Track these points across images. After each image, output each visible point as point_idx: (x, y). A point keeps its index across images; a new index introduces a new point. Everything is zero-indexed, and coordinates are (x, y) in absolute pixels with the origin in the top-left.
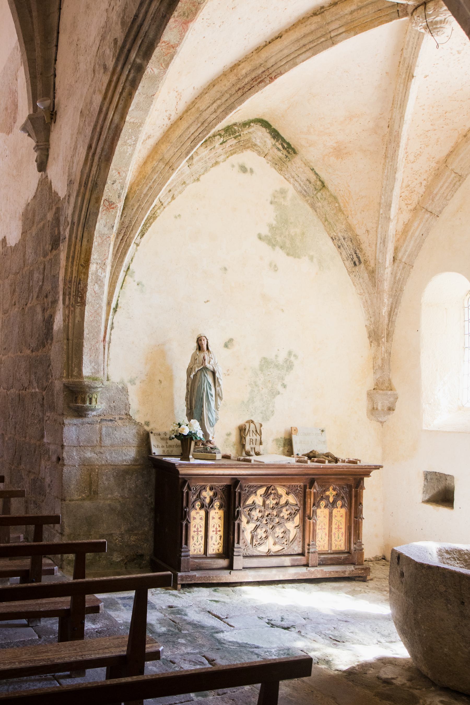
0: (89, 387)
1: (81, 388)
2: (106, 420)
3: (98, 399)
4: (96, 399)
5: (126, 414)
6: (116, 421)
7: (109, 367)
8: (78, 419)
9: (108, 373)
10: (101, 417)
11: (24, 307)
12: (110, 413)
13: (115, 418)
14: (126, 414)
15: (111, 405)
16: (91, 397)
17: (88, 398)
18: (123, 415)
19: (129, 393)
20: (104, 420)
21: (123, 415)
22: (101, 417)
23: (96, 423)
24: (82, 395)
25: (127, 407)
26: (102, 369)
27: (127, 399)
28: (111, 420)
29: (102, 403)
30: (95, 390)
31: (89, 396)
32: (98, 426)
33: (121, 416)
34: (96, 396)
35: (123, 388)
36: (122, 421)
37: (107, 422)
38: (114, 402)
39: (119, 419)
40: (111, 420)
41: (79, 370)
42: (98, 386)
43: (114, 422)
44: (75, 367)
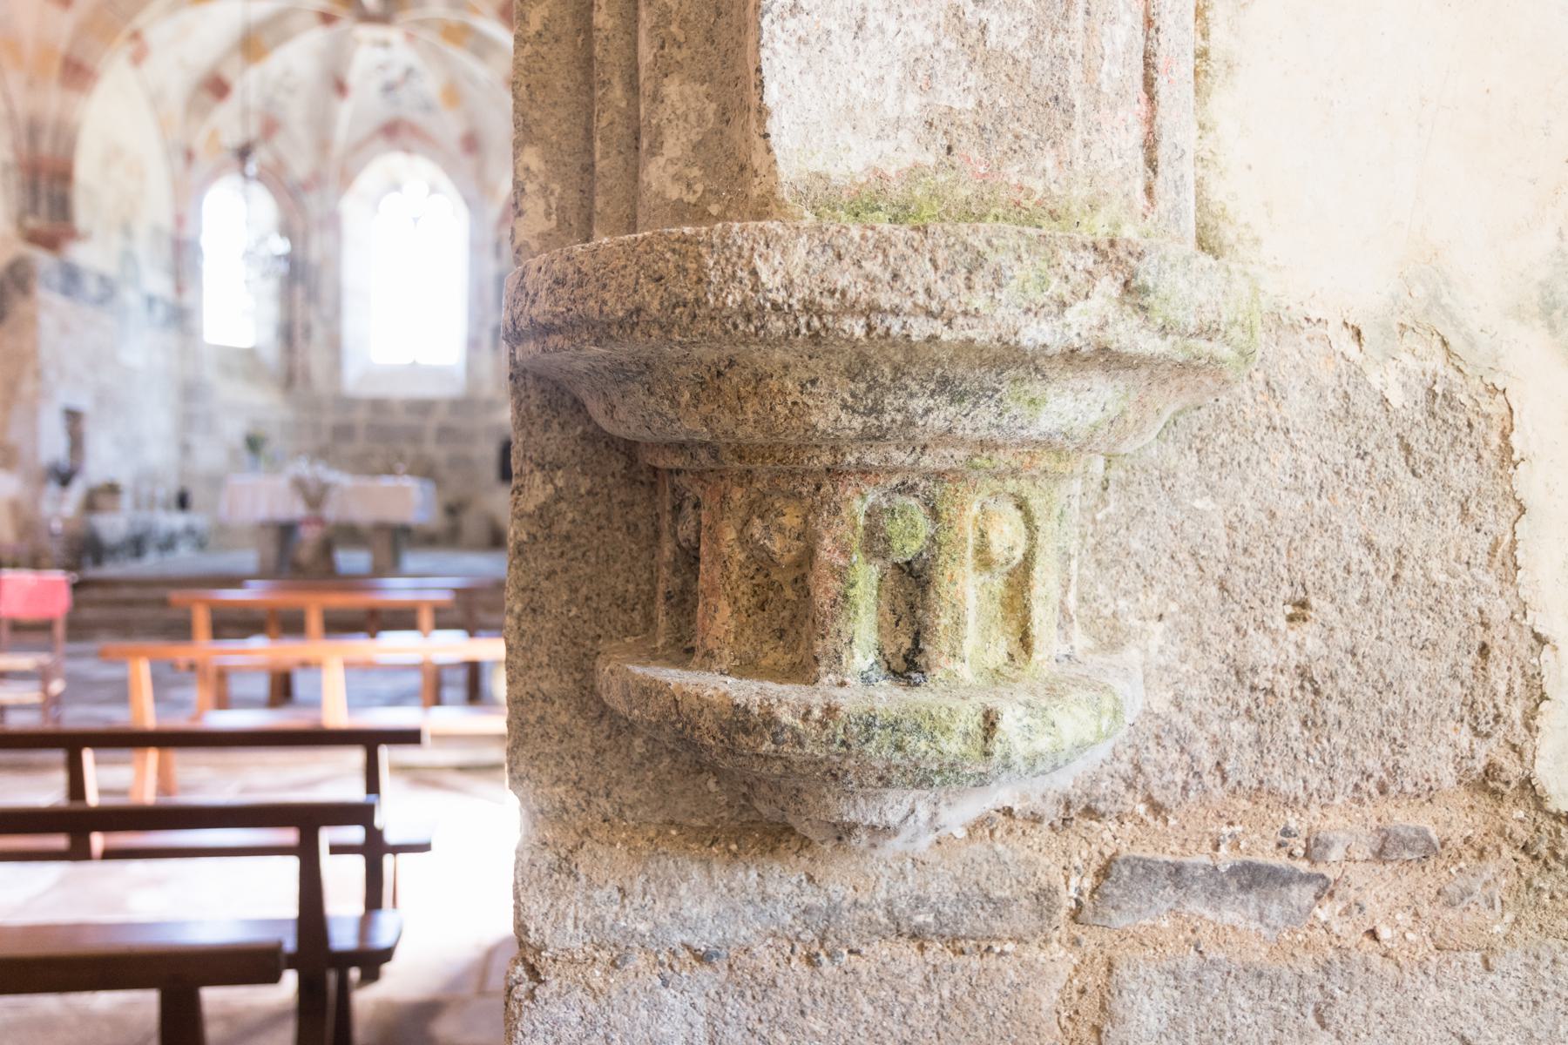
0: (859, 366)
1: (711, 381)
2: (1177, 872)
3: (1045, 583)
4: (1021, 577)
5: (1487, 783)
6: (1326, 890)
7: (1221, 103)
8: (747, 877)
9: (1218, 192)
10: (1108, 837)
11: (1382, 951)
12: (1241, 765)
13: (1315, 848)
14: (1487, 783)
15: (1262, 650)
16: (909, 548)
17: (867, 578)
18: (1429, 794)
19: (1527, 483)
20: (1147, 869)
21: (1429, 794)
22: (1108, 837)
23: (1022, 917)
24: (758, 508)
25: (1499, 677)
26: (1119, 72)
27: (1508, 563)
28: (1254, 877)
29: (1112, 639)
30: (980, 420)
31: (875, 541)
32: (1058, 960)
33: (1403, 818)
34: (1007, 535)
35: (1437, 399)
36: (1428, 879)
37: (1196, 907)
38: (1300, 610)
39: (1380, 855)
40: (1254, 877)
41: (724, 116)
42: (1035, 333)
43: (1302, 895)
44: (664, 70)
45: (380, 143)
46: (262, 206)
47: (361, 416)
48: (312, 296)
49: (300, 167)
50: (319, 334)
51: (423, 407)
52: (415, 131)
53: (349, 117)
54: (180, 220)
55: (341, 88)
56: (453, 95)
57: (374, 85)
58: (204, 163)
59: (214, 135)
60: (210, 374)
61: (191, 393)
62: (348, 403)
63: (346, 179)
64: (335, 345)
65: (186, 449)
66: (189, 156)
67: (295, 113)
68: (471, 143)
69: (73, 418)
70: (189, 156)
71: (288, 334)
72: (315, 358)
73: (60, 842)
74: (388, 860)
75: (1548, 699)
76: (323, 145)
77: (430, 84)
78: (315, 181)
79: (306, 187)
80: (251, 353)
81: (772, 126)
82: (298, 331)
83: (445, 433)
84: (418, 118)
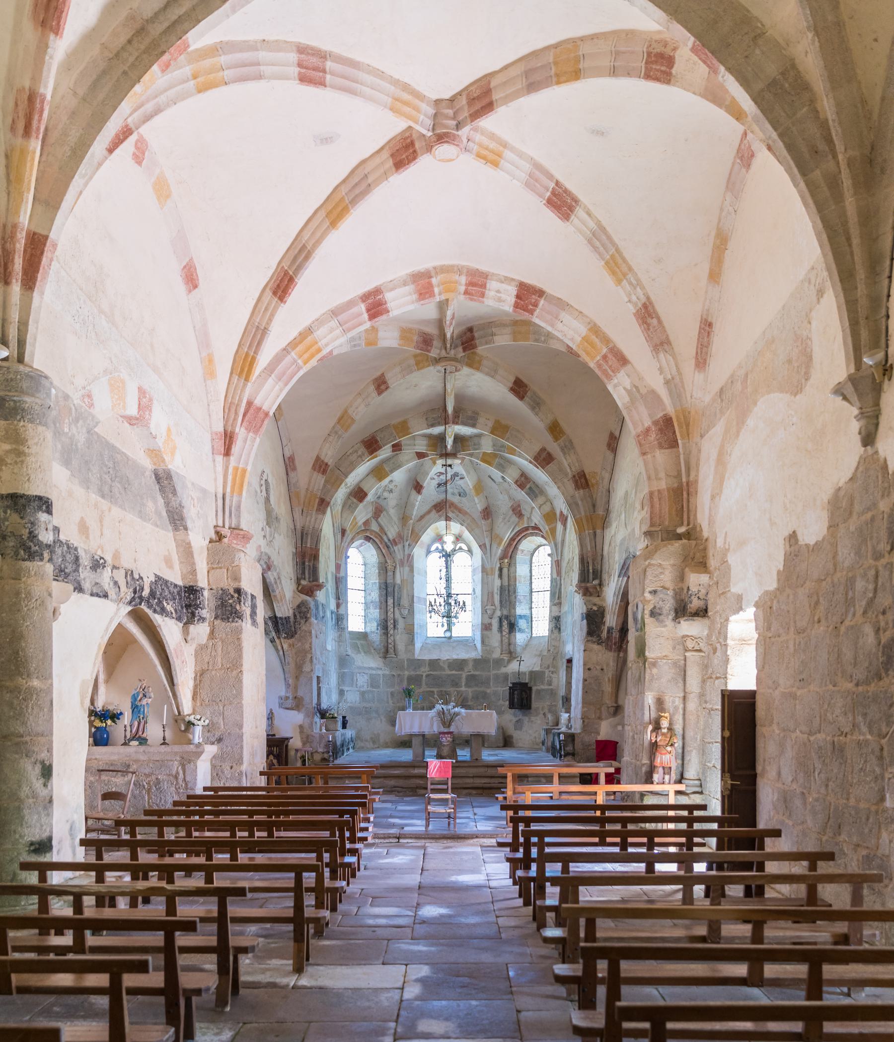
45: (434, 514)
46: (371, 553)
47: (424, 671)
48: (397, 604)
49: (392, 532)
50: (401, 624)
51: (460, 664)
52: (452, 505)
53: (420, 503)
54: (338, 567)
55: (418, 487)
56: (479, 488)
57: (434, 483)
58: (349, 535)
59: (355, 518)
60: (349, 652)
61: (343, 661)
62: (417, 664)
63: (416, 537)
64: (410, 631)
65: (341, 693)
66: (343, 532)
67: (392, 501)
68: (487, 513)
69: (318, 677)
70: (343, 532)
71: (385, 626)
72: (400, 639)
73: (596, 840)
74: (290, 913)
75: (162, 744)
76: (404, 519)
77: (468, 483)
78: (400, 539)
79: (394, 542)
80: (364, 636)
81: (757, 599)
82: (391, 626)
83: (471, 679)
84: (455, 499)
